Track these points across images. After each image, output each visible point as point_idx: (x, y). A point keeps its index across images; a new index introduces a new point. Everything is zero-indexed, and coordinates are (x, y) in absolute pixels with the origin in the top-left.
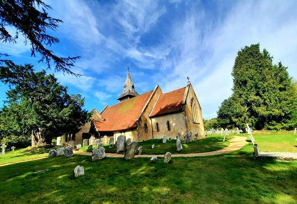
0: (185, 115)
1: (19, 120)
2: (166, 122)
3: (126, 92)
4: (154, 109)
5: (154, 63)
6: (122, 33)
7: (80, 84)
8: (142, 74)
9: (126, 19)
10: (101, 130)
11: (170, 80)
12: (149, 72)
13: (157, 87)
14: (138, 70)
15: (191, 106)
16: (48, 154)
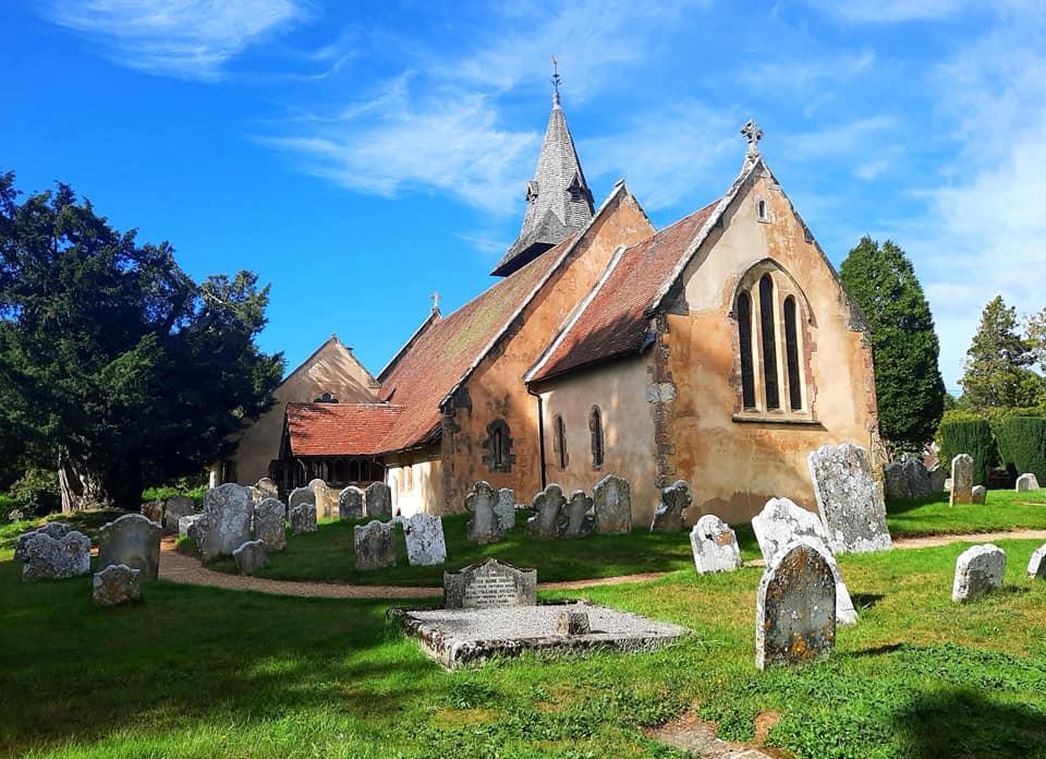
0: (660, 377)
4: (545, 343)
7: (476, 180)
8: (863, 62)
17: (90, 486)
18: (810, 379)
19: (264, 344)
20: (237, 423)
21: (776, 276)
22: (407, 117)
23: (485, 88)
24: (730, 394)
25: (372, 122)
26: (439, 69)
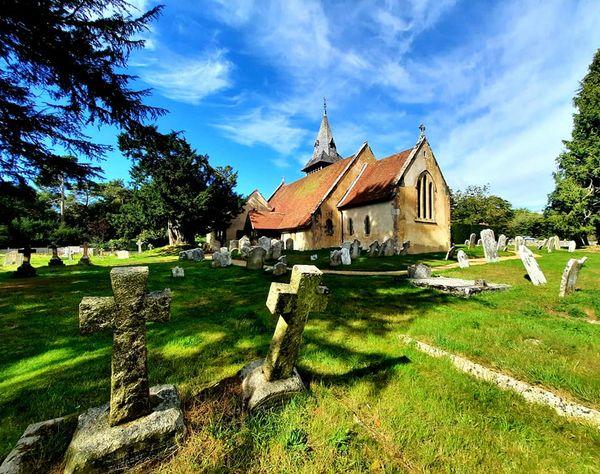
1: (145, 208)
2: (364, 218)
3: (316, 155)
5: (433, 91)
6: (376, 37)
7: (278, 143)
8: (402, 115)
9: (391, 8)
10: (260, 227)
11: (462, 121)
12: (417, 110)
13: (364, 149)
14: (395, 106)
15: (418, 188)
16: (177, 258)
17: (180, 237)
18: (435, 209)
19: (237, 190)
20: (229, 217)
21: (428, 175)
22: (259, 120)
23: (286, 114)
24: (415, 213)
25: (247, 121)
26: (273, 106)
